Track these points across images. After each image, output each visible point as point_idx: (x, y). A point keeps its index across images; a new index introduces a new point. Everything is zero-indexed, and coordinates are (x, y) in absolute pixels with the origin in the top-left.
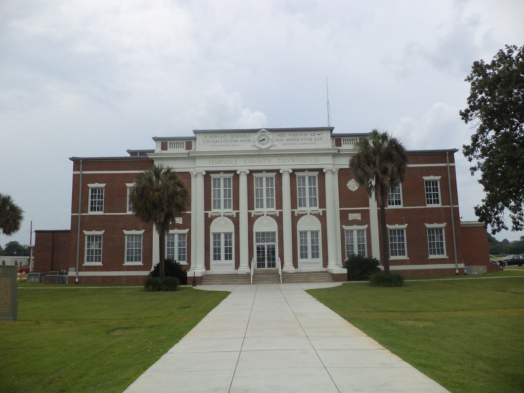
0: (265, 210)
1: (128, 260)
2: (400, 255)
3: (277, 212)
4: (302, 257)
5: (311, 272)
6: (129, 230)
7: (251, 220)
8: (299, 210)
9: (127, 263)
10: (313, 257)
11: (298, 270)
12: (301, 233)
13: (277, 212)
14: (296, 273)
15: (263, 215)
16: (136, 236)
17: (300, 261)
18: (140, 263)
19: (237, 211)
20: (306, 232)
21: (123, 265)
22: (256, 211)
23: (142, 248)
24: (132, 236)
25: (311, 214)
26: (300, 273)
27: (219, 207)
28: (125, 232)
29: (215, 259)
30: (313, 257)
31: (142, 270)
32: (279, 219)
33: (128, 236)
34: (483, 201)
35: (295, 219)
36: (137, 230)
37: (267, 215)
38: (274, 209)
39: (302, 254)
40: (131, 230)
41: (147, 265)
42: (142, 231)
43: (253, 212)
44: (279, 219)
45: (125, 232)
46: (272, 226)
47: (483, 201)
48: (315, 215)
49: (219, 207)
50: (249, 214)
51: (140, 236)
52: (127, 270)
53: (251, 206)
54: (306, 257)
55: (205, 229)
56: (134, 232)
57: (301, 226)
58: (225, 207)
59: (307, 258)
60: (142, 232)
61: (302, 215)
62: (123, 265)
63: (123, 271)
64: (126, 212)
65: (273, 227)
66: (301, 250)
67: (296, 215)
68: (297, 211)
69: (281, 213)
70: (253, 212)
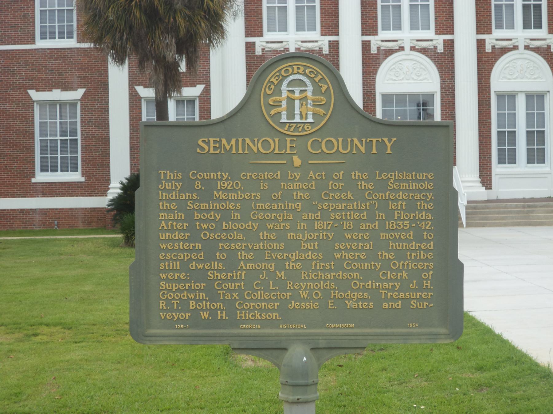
0: (406, 35)
1: (44, 169)
2: (64, 169)
3: (439, 41)
4: (501, 161)
5: (532, 200)
6: (44, 90)
7: (371, 62)
8: (495, 37)
9: (41, 177)
10: (530, 160)
11: (492, 194)
12: (500, 96)
13: (439, 41)
14: (488, 201)
15: (402, 49)
16: (62, 104)
17: (497, 169)
18: (76, 177)
19: (333, 38)
20: (512, 96)
21: (33, 180)
22: (382, 37)
23: (79, 137)
24: (52, 104)
25: (527, 48)
26: (498, 201)
27: (284, 28)
28: (34, 95)
29: (501, 161)
30: (530, 160)
31: (83, 195)
32: (445, 61)
33: (42, 104)
34: (126, 179)
35: (486, 60)
36: (65, 89)
37: (413, 49)
38: (430, 34)
39: (501, 152)
40: (50, 90)
41: (97, 182)
42: (78, 94)
43: (375, 41)
44: (445, 61)
45: (34, 95)
46: (428, 81)
47: (126, 179)
48: (537, 50)
49: (284, 28)
50: (366, 46)
51: (73, 104)
52: (44, 195)
53: (369, 26)
54: (513, 160)
55: (297, 25)
56: (57, 95)
57: (501, 79)
58: (300, 27)
59: (544, 162)
60: (78, 94)
61: (504, 51)
62: (33, 180)
63: (32, 196)
64: (33, 42)
65: (428, 81)
66: (501, 142)
67: (488, 49)
68: (491, 40)
69: (450, 45)
70: (375, 41)
